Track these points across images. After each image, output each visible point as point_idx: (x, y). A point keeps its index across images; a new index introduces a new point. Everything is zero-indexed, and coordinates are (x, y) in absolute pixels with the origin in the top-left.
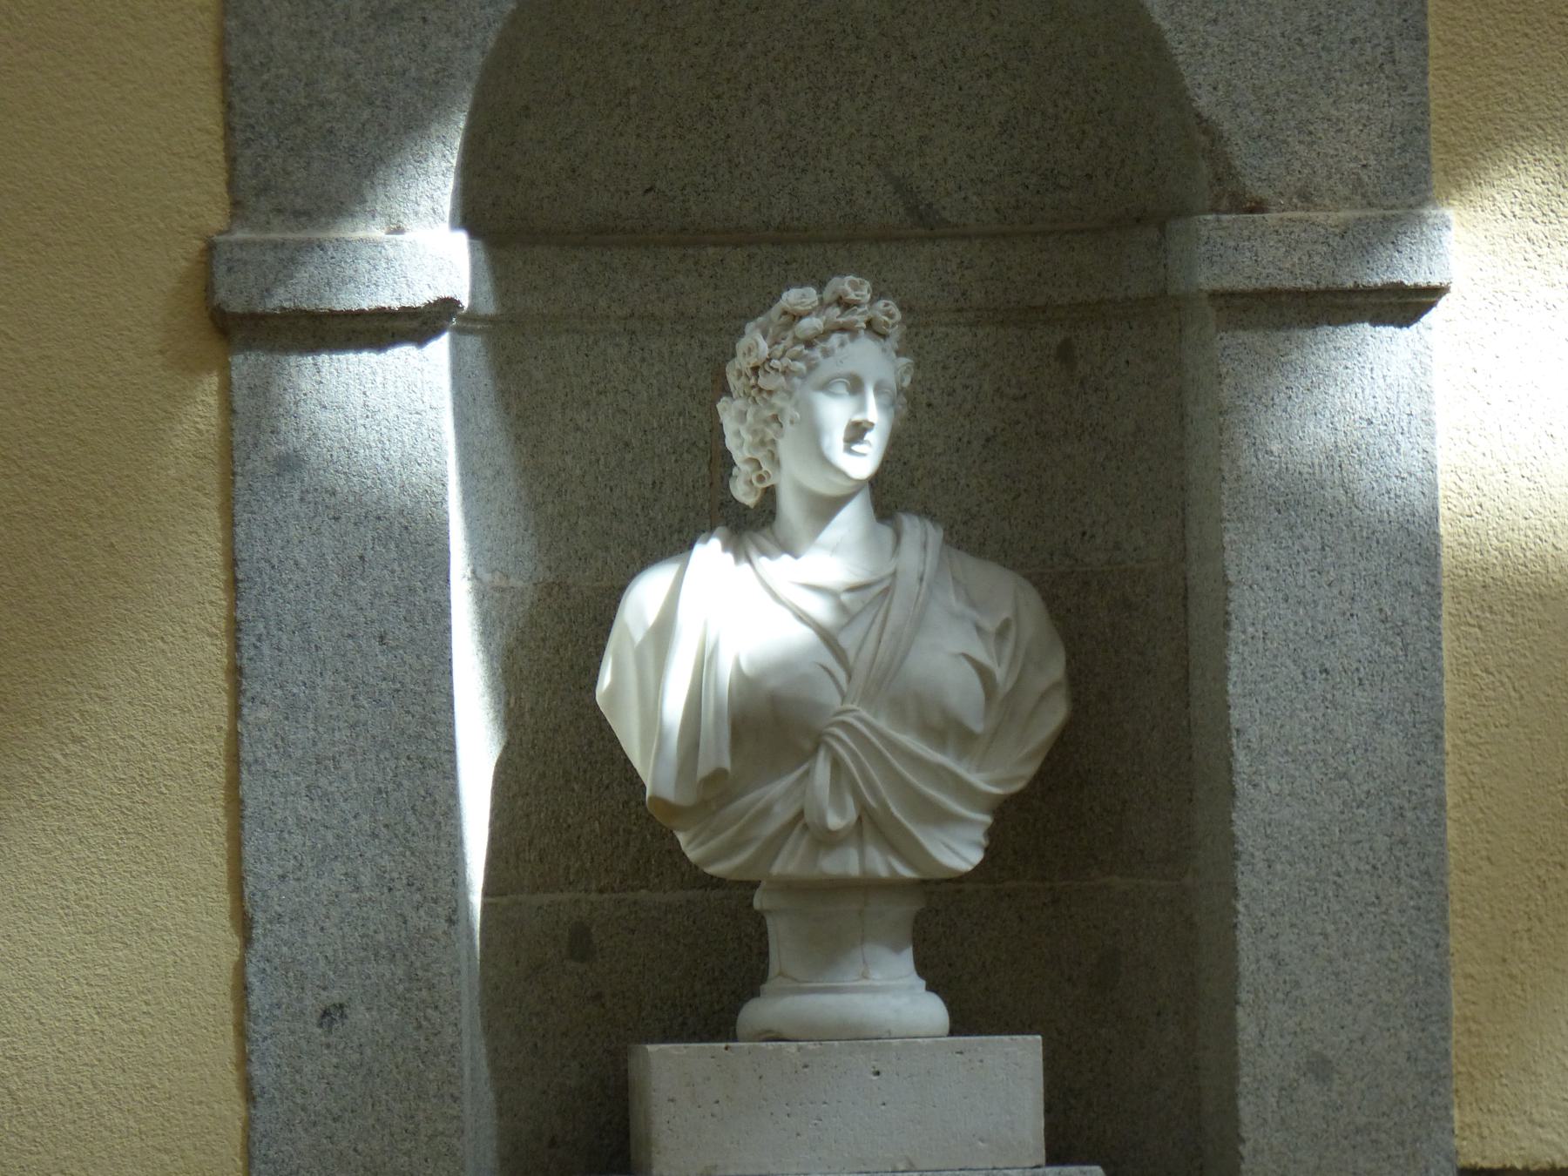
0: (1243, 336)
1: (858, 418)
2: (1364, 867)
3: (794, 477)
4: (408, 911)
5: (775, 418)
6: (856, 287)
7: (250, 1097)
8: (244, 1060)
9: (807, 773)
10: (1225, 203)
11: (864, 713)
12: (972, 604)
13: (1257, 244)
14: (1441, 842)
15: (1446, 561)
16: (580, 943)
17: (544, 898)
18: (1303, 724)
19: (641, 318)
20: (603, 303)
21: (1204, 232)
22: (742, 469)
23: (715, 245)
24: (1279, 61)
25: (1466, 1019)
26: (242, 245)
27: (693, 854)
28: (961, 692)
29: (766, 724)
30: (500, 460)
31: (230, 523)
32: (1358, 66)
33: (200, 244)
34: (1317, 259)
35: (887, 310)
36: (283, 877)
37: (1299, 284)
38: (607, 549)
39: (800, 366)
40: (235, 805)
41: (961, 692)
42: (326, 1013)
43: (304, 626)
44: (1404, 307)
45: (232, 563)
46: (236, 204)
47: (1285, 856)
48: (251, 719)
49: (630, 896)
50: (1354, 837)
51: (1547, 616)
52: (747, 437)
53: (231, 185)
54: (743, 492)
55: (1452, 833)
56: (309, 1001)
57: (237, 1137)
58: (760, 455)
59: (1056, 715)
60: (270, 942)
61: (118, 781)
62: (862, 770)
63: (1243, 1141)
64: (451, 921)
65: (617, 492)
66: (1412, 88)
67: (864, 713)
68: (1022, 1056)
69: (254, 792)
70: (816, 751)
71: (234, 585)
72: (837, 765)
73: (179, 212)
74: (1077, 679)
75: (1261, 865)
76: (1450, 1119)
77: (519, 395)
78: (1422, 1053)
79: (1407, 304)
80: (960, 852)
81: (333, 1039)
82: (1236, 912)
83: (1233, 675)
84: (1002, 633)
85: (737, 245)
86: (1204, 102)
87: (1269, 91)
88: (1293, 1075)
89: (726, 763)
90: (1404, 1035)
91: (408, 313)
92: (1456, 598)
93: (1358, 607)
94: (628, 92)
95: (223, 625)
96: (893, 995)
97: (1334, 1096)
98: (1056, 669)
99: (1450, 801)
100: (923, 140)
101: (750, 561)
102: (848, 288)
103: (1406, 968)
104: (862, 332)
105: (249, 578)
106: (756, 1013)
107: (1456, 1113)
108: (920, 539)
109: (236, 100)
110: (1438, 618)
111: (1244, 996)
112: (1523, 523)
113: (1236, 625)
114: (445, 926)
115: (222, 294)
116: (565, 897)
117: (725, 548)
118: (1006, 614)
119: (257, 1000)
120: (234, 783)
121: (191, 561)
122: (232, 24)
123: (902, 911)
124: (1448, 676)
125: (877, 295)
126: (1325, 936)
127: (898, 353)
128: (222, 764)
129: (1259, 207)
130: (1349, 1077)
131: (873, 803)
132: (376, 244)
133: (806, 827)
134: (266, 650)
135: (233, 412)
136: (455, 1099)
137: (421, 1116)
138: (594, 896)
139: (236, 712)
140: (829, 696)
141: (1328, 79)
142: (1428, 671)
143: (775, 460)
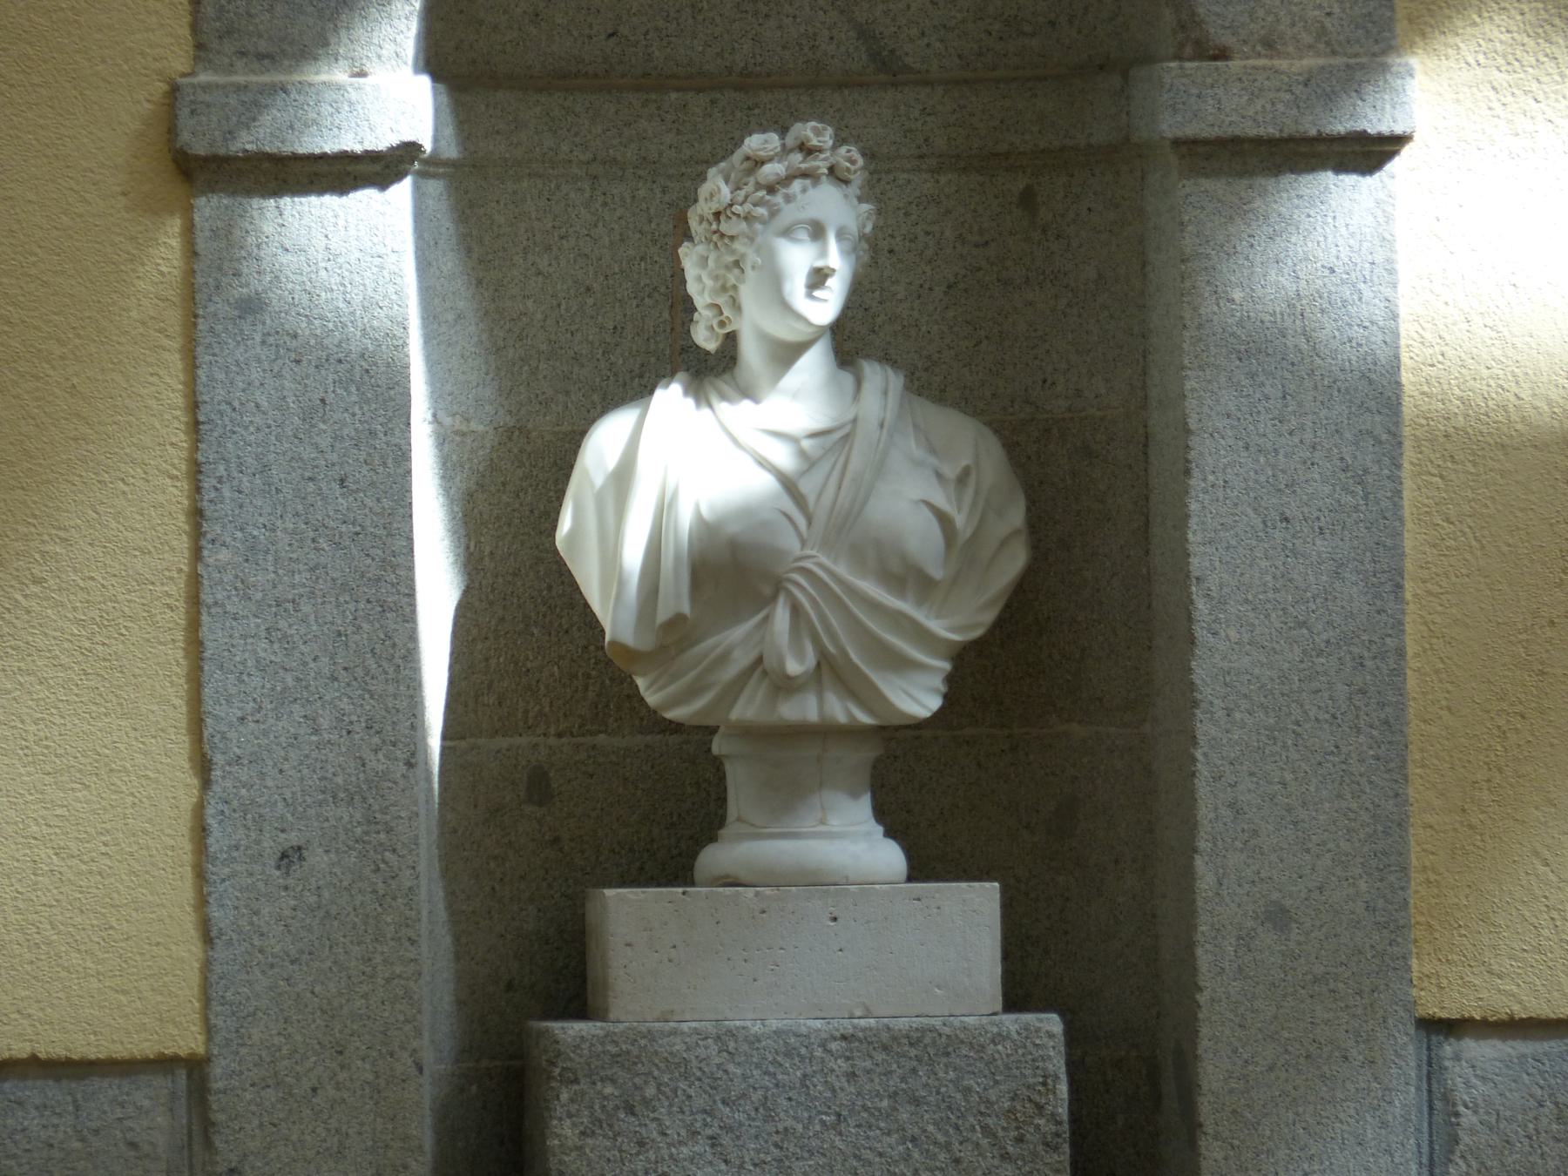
0: (1206, 184)
1: (819, 264)
2: (1323, 716)
3: (755, 324)
4: (368, 755)
5: (737, 264)
6: (818, 133)
7: (208, 939)
8: (202, 902)
9: (766, 619)
10: (1188, 50)
11: (824, 560)
12: (933, 451)
13: (1220, 91)
14: (1401, 691)
15: (1408, 409)
16: (539, 786)
17: (502, 742)
20: (565, 148)
21: (1167, 79)
22: (704, 315)
23: (678, 90)
26: (206, 88)
27: (652, 699)
28: (920, 538)
29: (726, 570)
30: (461, 304)
31: (192, 366)
33: (164, 87)
34: (1281, 107)
35: (850, 156)
37: (1262, 131)
39: (761, 211)
40: (195, 646)
41: (920, 538)
42: (284, 856)
44: (1367, 155)
45: (194, 406)
46: (199, 46)
49: (588, 740)
50: (1315, 685)
52: (709, 283)
53: (195, 28)
54: (704, 337)
55: (1412, 682)
57: (195, 978)
58: (721, 300)
59: (1015, 562)
60: (228, 783)
61: (78, 621)
63: (1200, 989)
67: (824, 560)
69: (212, 632)
71: (195, 426)
73: (143, 54)
74: (1036, 526)
75: (1220, 713)
76: (1409, 969)
78: (1381, 903)
79: (1371, 152)
80: (918, 698)
81: (290, 882)
82: (1194, 760)
83: (1193, 523)
84: (962, 479)
85: (699, 90)
88: (1250, 924)
89: (686, 608)
90: (1363, 886)
91: (371, 157)
92: (1418, 448)
96: (851, 841)
97: (1292, 945)
98: (1017, 516)
101: (710, 406)
102: (810, 133)
103: (1365, 817)
104: (824, 178)
105: (210, 421)
107: (1414, 963)
110: (1399, 467)
111: (1202, 845)
112: (1485, 373)
113: (1196, 473)
114: (403, 768)
115: (185, 136)
117: (686, 392)
119: (215, 842)
120: (194, 624)
121: (152, 402)
123: (863, 756)
124: (1409, 525)
125: (840, 141)
126: (1285, 785)
127: (860, 199)
128: (181, 605)
129: (1222, 54)
131: (832, 649)
132: (339, 87)
133: (765, 673)
134: (227, 493)
135: (196, 254)
137: (378, 959)
138: (552, 741)
139: (197, 554)
143: (736, 306)
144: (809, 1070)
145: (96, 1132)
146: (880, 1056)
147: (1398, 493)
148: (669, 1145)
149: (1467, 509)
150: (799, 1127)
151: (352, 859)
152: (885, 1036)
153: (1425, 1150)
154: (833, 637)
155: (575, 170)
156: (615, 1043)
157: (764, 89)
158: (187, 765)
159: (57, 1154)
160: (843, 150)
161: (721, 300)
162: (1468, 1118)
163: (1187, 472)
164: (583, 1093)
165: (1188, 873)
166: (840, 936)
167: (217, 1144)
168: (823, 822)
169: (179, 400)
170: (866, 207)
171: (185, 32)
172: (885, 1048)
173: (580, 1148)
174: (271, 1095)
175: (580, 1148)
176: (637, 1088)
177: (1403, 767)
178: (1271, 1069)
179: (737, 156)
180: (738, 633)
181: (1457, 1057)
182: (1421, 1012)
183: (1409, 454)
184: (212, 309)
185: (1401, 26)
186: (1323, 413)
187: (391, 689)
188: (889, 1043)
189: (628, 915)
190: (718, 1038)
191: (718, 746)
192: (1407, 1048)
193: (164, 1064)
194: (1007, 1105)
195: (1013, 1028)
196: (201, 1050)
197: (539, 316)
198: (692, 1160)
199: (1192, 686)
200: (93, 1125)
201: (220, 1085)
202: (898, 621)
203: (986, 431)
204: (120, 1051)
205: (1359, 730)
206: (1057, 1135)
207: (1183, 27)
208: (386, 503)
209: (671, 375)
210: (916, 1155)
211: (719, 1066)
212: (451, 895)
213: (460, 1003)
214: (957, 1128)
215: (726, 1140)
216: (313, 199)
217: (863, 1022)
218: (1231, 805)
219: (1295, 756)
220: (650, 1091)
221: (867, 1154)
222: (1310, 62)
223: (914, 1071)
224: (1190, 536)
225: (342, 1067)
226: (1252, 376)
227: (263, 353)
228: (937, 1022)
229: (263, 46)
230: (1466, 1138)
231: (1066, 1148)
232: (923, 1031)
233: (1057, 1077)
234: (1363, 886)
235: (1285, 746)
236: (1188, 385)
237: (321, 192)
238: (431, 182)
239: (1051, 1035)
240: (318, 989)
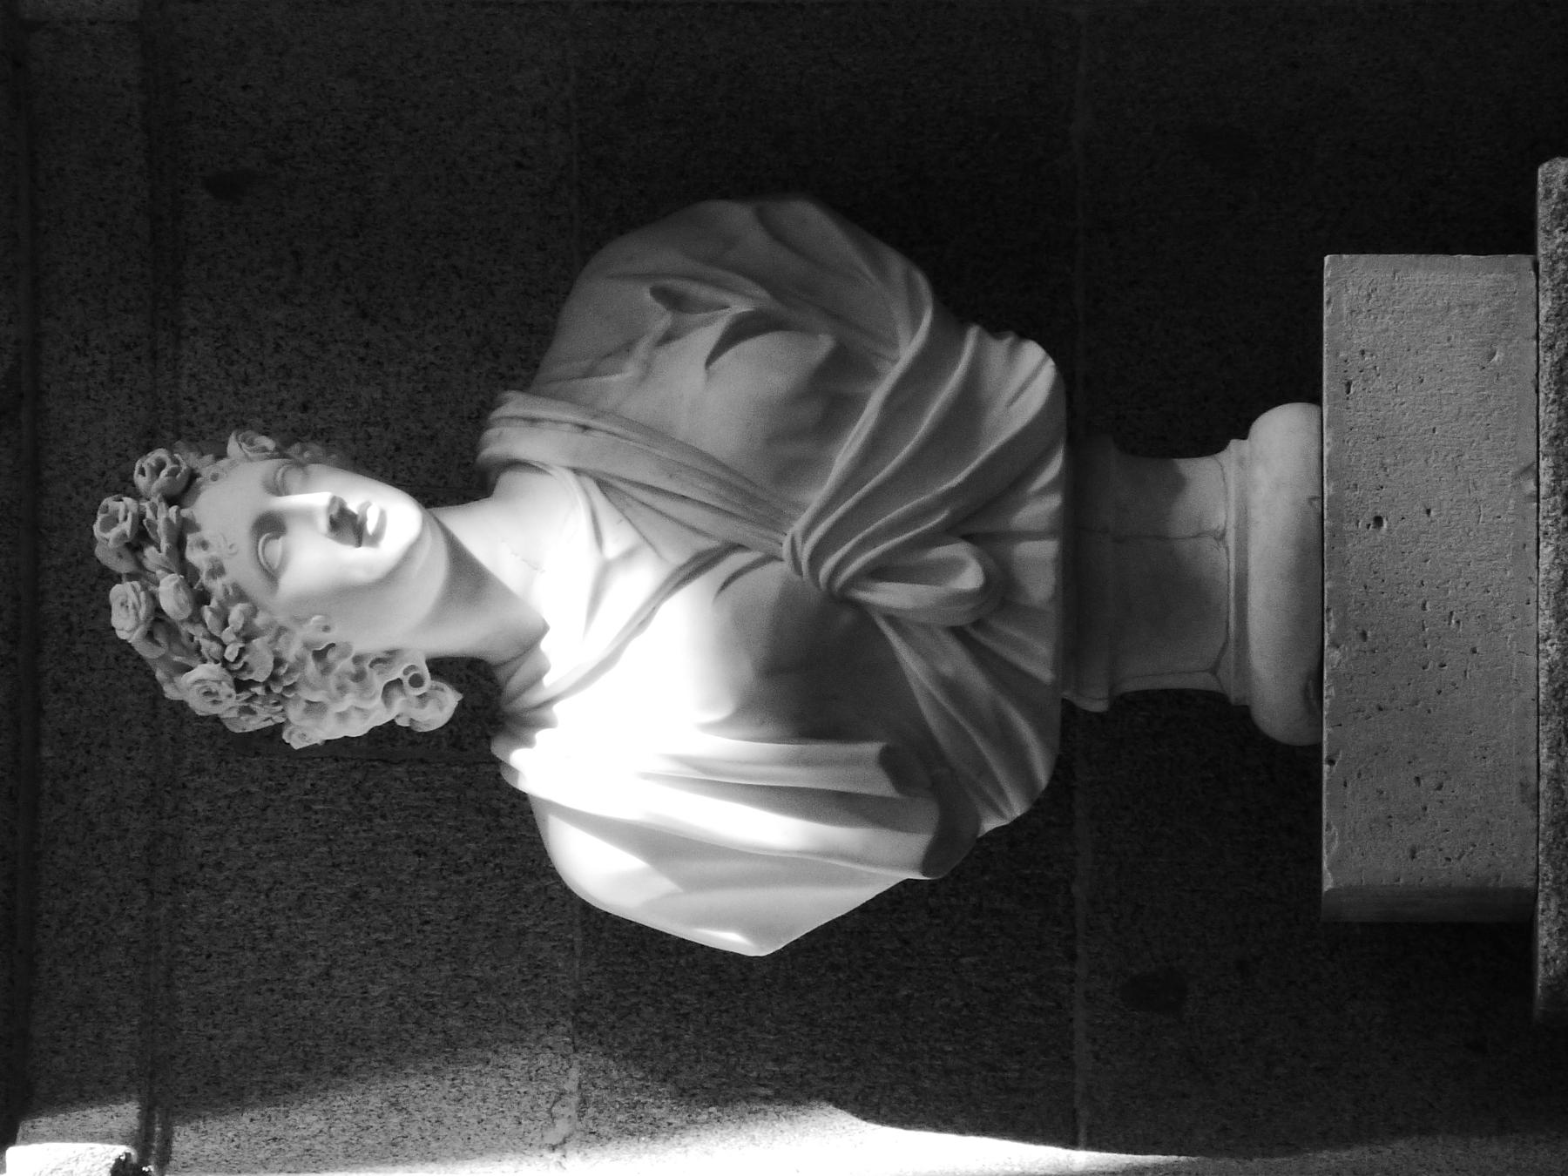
1: (323, 523)
3: (417, 627)
5: (320, 655)
6: (112, 521)
9: (893, 619)
11: (798, 526)
12: (628, 347)
20: (126, 929)
23: (37, 745)
29: (813, 677)
30: (375, 1101)
39: (236, 614)
52: (349, 701)
54: (436, 710)
59: (809, 219)
65: (431, 913)
67: (798, 526)
70: (863, 611)
72: (879, 572)
74: (756, 183)
80: (1026, 380)
84: (675, 301)
89: (872, 749)
96: (1256, 487)
98: (737, 216)
102: (114, 533)
104: (185, 512)
117: (528, 743)
125: (126, 487)
127: (221, 455)
133: (979, 624)
140: (771, 579)
143: (387, 658)
160: (141, 481)
168: (1221, 537)
189: (1362, 850)
217: (1546, 479)
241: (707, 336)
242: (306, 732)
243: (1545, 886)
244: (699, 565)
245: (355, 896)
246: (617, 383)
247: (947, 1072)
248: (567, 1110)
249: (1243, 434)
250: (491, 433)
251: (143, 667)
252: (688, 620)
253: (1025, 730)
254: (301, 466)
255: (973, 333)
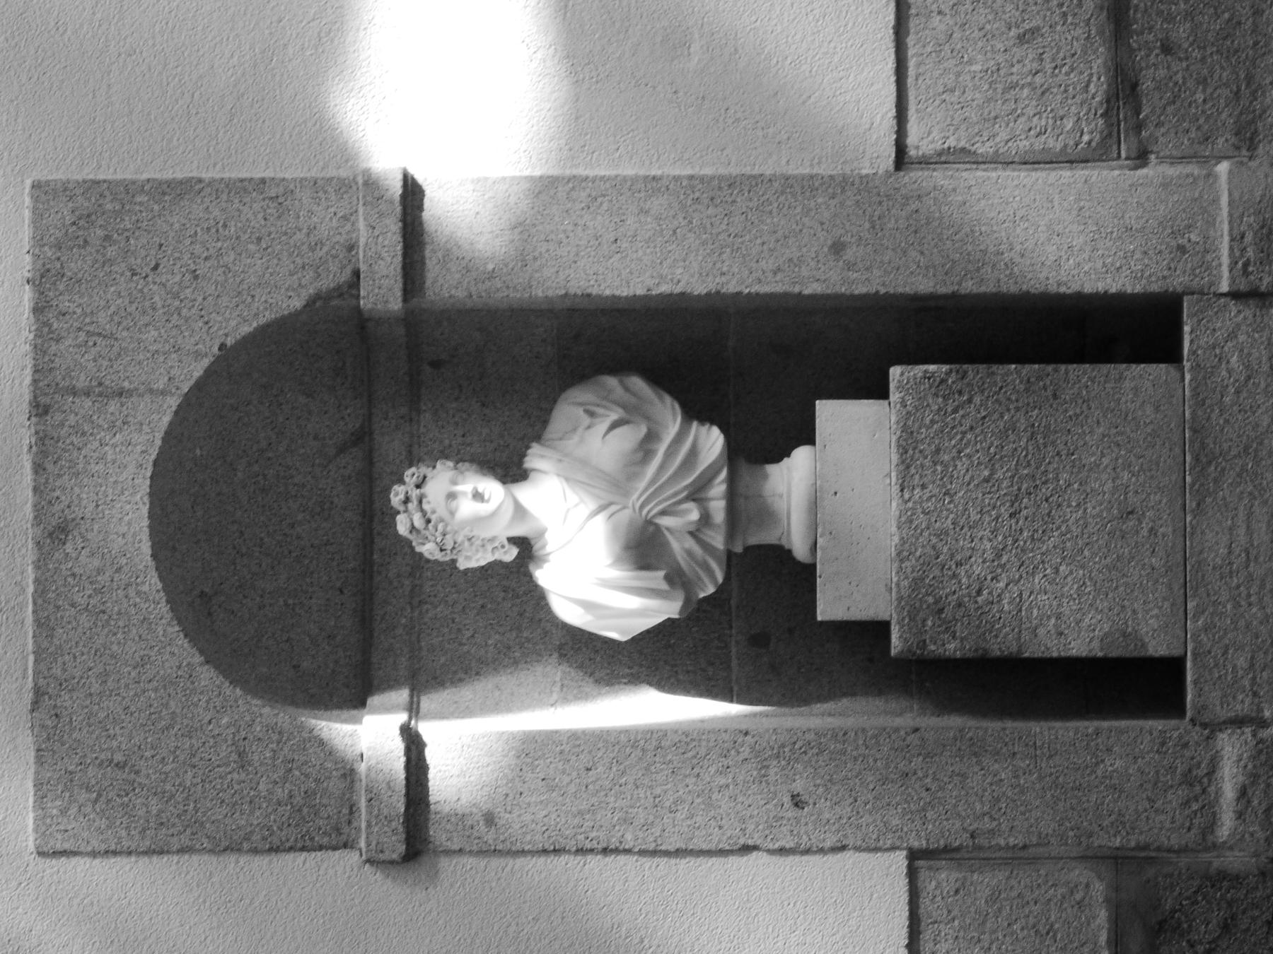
0: (428, 283)
1: (470, 496)
2: (725, 221)
3: (504, 528)
4: (741, 758)
5: (469, 540)
6: (397, 494)
7: (843, 848)
8: (821, 851)
9: (668, 529)
10: (354, 292)
11: (635, 496)
12: (575, 430)
13: (377, 276)
14: (713, 178)
15: (555, 172)
16: (759, 640)
17: (734, 663)
18: (645, 254)
19: (412, 598)
20: (404, 621)
21: (369, 306)
22: (499, 556)
23: (372, 554)
24: (275, 261)
25: (812, 165)
26: (368, 845)
27: (711, 590)
28: (627, 437)
29: (643, 549)
30: (490, 686)
31: (523, 853)
32: (279, 217)
33: (367, 865)
34: (386, 243)
35: (411, 475)
36: (720, 827)
37: (400, 253)
38: (540, 620)
39: (440, 527)
40: (679, 853)
41: (627, 437)
42: (796, 805)
43: (580, 813)
44: (414, 193)
45: (545, 852)
46: (345, 846)
47: (718, 265)
48: (631, 844)
49: (733, 609)
50: (709, 226)
51: (587, 115)
52: (480, 555)
53: (335, 848)
54: (511, 554)
55: (708, 171)
56: (789, 814)
57: (864, 855)
58: (489, 547)
59: (637, 383)
60: (756, 836)
61: (665, 918)
62: (665, 500)
63: (877, 292)
64: (746, 734)
65: (509, 613)
66: (292, 187)
67: (635, 496)
68: (828, 412)
69: (672, 844)
70: (657, 526)
71: (556, 851)
72: (663, 513)
73: (349, 877)
74: (618, 368)
75: (724, 279)
76: (867, 176)
77: (455, 672)
78: (830, 190)
79: (412, 192)
80: (712, 441)
81: (811, 801)
82: (749, 293)
83: (617, 293)
84: (591, 414)
85: (372, 542)
86: (297, 304)
87: (292, 266)
88: (841, 263)
89: (661, 574)
90: (820, 200)
91: (408, 751)
92: (577, 166)
93: (581, 222)
94: (286, 604)
95: (579, 858)
96: (791, 479)
97: (853, 240)
98: (612, 382)
99: (689, 172)
100: (316, 438)
101: (548, 554)
102: (397, 499)
103: (782, 199)
104: (422, 491)
105: (553, 843)
106: (800, 550)
107: (864, 172)
108: (536, 459)
109: (288, 845)
110: (587, 178)
111: (797, 289)
112: (535, 128)
113: (589, 291)
114: (748, 738)
115: (395, 856)
116: (734, 650)
117: (541, 567)
118: (580, 411)
119: (790, 844)
120: (667, 854)
121: (543, 876)
122: (246, 846)
123: (744, 469)
124: (620, 172)
125: (401, 481)
126: (763, 243)
127: (434, 467)
128: (657, 860)
129: (357, 274)
130: (843, 231)
131: (685, 494)
132: (369, 769)
133: (698, 530)
134: (593, 834)
135: (460, 850)
136: (845, 734)
137: (855, 753)
138: (734, 631)
139: (628, 851)
140: (626, 515)
141: (286, 234)
142: (618, 184)
143: (492, 540)
144: (920, 510)
145: (949, 912)
146: (913, 471)
147: (602, 178)
148: (961, 589)
149: (611, 139)
150: (952, 516)
151: (799, 767)
152: (902, 467)
153: (968, 166)
154: (676, 494)
155: (416, 614)
156: (903, 619)
157: (374, 516)
158: (745, 858)
159: (961, 934)
160: (407, 479)
161: (489, 547)
162: (951, 142)
163: (589, 295)
164: (931, 638)
165: (813, 297)
166: (847, 480)
167: (957, 844)
168: (781, 496)
169: (542, 859)
170: (439, 465)
171: (337, 853)
172: (908, 467)
173: (962, 639)
174: (930, 814)
175: (962, 639)
176: (928, 607)
177: (754, 177)
178: (922, 253)
179: (410, 537)
180: (675, 545)
181: (917, 148)
182: (892, 168)
183: (581, 171)
184: (491, 842)
185: (343, 173)
186: (556, 219)
187: (704, 743)
188: (905, 465)
189: (831, 605)
190: (902, 561)
191: (738, 549)
192: (913, 176)
193: (912, 873)
194: (940, 400)
195: (898, 395)
196: (905, 853)
197: (497, 636)
198: (969, 577)
199: (708, 295)
200: (945, 912)
201: (924, 842)
202: (670, 453)
203: (563, 396)
204: (904, 898)
205: (734, 202)
206: (957, 372)
207: (341, 295)
208: (600, 745)
209: (530, 576)
210: (968, 451)
211: (917, 560)
212: (822, 699)
213: (880, 693)
214: (953, 428)
215: (959, 557)
216: (430, 784)
217: (894, 479)
218: (775, 273)
219: (747, 237)
220: (931, 600)
221: (967, 478)
222: (361, 225)
223: (921, 452)
224: (625, 294)
225: (915, 773)
226: (535, 259)
227: (516, 812)
228: (894, 439)
229: (345, 811)
230: (962, 144)
231: (965, 366)
232: (899, 446)
233: (926, 371)
234: (820, 200)
235: (742, 243)
236: (540, 294)
237: (427, 780)
238: (422, 705)
239: (902, 374)
240: (871, 787)
241: (603, 426)
242: (463, 565)
243: (893, 623)
244: (602, 508)
245: (482, 606)
246: (571, 444)
247: (688, 672)
248: (557, 688)
249: (788, 455)
250: (527, 459)
251: (409, 543)
252: (600, 525)
253: (714, 565)
254: (462, 473)
255: (695, 424)
